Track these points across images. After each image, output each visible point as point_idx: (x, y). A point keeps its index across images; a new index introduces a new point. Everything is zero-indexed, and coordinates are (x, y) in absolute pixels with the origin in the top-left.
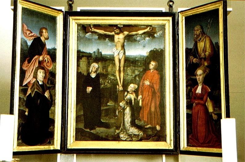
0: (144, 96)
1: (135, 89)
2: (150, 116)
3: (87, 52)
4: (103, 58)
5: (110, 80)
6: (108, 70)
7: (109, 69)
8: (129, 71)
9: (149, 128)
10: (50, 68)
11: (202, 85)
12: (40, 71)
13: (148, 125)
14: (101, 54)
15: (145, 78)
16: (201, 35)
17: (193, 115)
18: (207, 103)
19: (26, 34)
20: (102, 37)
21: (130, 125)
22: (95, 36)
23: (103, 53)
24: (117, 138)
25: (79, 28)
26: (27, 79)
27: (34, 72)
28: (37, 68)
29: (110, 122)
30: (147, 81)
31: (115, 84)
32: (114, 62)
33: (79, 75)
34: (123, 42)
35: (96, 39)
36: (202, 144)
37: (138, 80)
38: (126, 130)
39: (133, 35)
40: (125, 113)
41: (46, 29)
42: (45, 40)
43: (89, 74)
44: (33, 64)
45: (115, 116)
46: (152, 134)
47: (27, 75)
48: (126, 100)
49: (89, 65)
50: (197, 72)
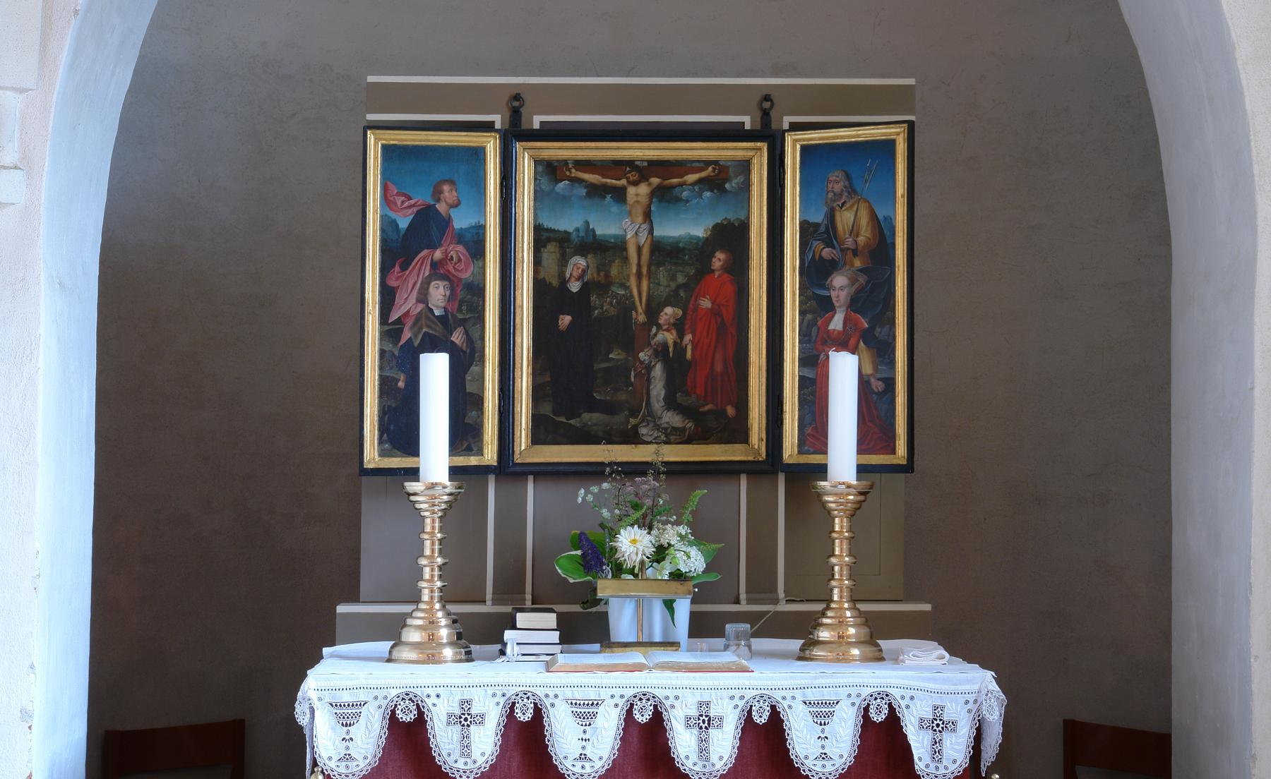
3: (560, 229)
5: (616, 298)
6: (610, 272)
8: (662, 275)
9: (710, 411)
10: (466, 276)
11: (847, 312)
12: (438, 284)
13: (707, 405)
16: (846, 194)
19: (395, 204)
20: (596, 192)
21: (663, 406)
23: (598, 232)
24: (632, 438)
25: (540, 169)
26: (401, 306)
27: (420, 289)
30: (706, 300)
31: (627, 307)
32: (625, 253)
33: (540, 287)
37: (684, 297)
39: (673, 187)
40: (652, 376)
41: (452, 183)
43: (564, 282)
44: (416, 271)
47: (399, 299)
48: (655, 347)
49: (563, 260)
50: (831, 281)
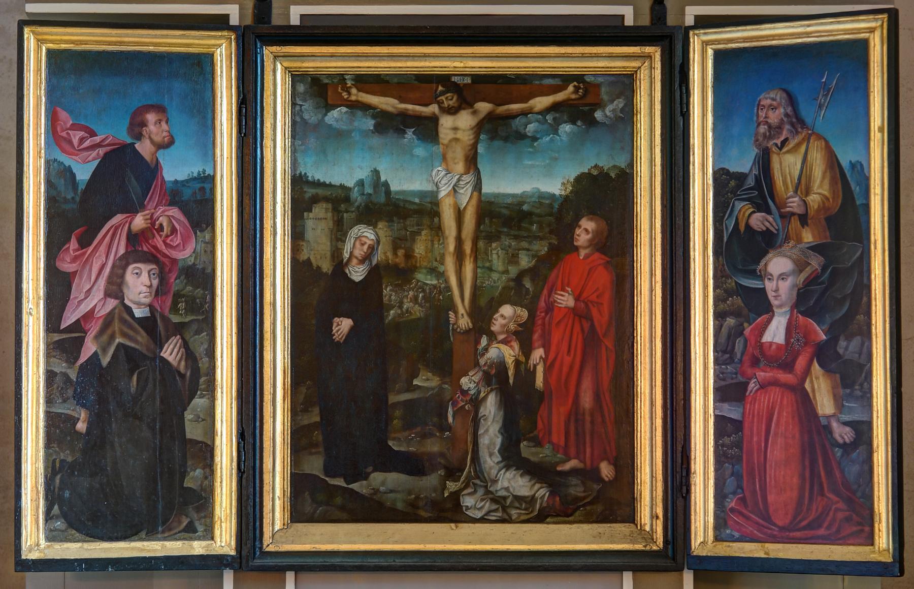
0: (553, 348)
1: (519, 325)
2: (576, 429)
4: (396, 206)
5: (424, 291)
6: (413, 251)
7: (420, 249)
9: (574, 472)
14: (388, 192)
15: (559, 283)
16: (787, 127)
17: (746, 425)
18: (812, 382)
21: (498, 463)
22: (364, 120)
23: (394, 187)
25: (301, 88)
28: (121, 258)
29: (422, 450)
32: (436, 220)
34: (472, 142)
35: (365, 134)
36: (782, 529)
38: (486, 482)
39: (512, 116)
41: (160, 109)
42: (156, 152)
43: (340, 266)
44: (103, 248)
45: (443, 427)
46: (582, 495)
47: (76, 293)
49: (339, 232)
50: (766, 265)
